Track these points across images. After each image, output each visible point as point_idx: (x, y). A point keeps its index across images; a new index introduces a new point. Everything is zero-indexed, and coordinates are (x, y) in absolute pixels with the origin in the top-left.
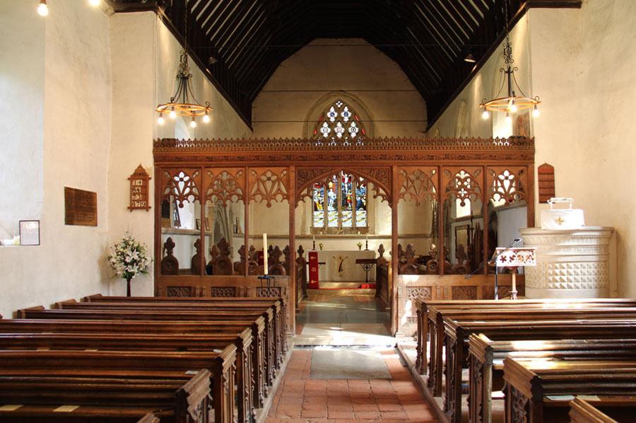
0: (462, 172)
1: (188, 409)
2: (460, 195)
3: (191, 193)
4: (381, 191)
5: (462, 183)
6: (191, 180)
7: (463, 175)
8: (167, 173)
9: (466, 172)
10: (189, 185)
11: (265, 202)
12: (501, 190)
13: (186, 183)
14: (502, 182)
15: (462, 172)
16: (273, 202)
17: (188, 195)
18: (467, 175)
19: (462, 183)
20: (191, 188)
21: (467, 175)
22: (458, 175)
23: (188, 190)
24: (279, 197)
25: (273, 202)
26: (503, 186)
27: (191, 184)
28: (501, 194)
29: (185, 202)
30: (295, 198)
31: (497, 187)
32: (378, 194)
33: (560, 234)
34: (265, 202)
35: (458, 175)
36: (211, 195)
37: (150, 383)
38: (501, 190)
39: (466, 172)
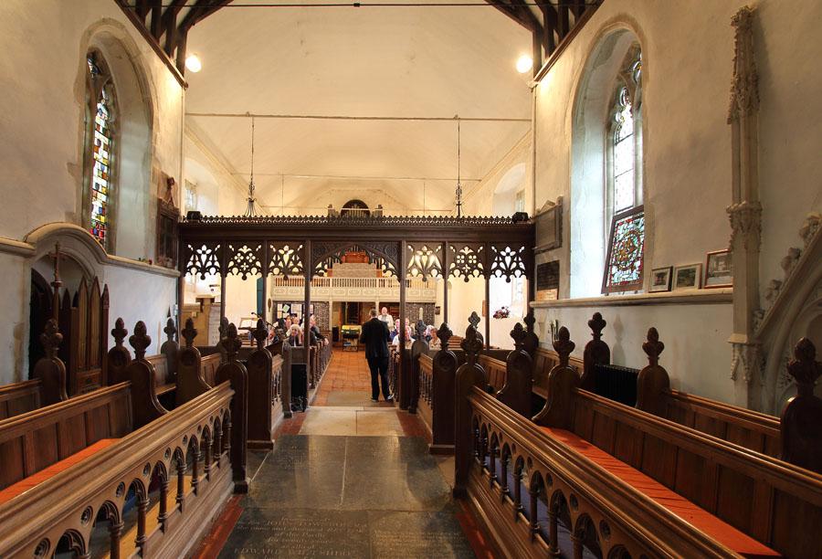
0: (466, 248)
1: (815, 395)
2: (464, 271)
3: (518, 267)
4: (391, 266)
5: (245, 258)
6: (212, 253)
7: (467, 251)
8: (452, 248)
9: (470, 248)
10: (211, 259)
11: (200, 274)
12: (198, 264)
13: (513, 258)
14: (503, 258)
15: (466, 248)
16: (511, 277)
17: (514, 270)
18: (249, 249)
19: (245, 258)
20: (518, 262)
21: (249, 249)
22: (241, 249)
23: (514, 265)
24: (213, 270)
25: (470, 277)
26: (200, 260)
27: (296, 258)
28: (502, 270)
29: (207, 274)
30: (309, 273)
31: (194, 261)
32: (388, 269)
33: (619, 305)
34: (200, 274)
35: (462, 251)
36: (453, 269)
37: (132, 438)
38: (198, 264)
39: (470, 248)
